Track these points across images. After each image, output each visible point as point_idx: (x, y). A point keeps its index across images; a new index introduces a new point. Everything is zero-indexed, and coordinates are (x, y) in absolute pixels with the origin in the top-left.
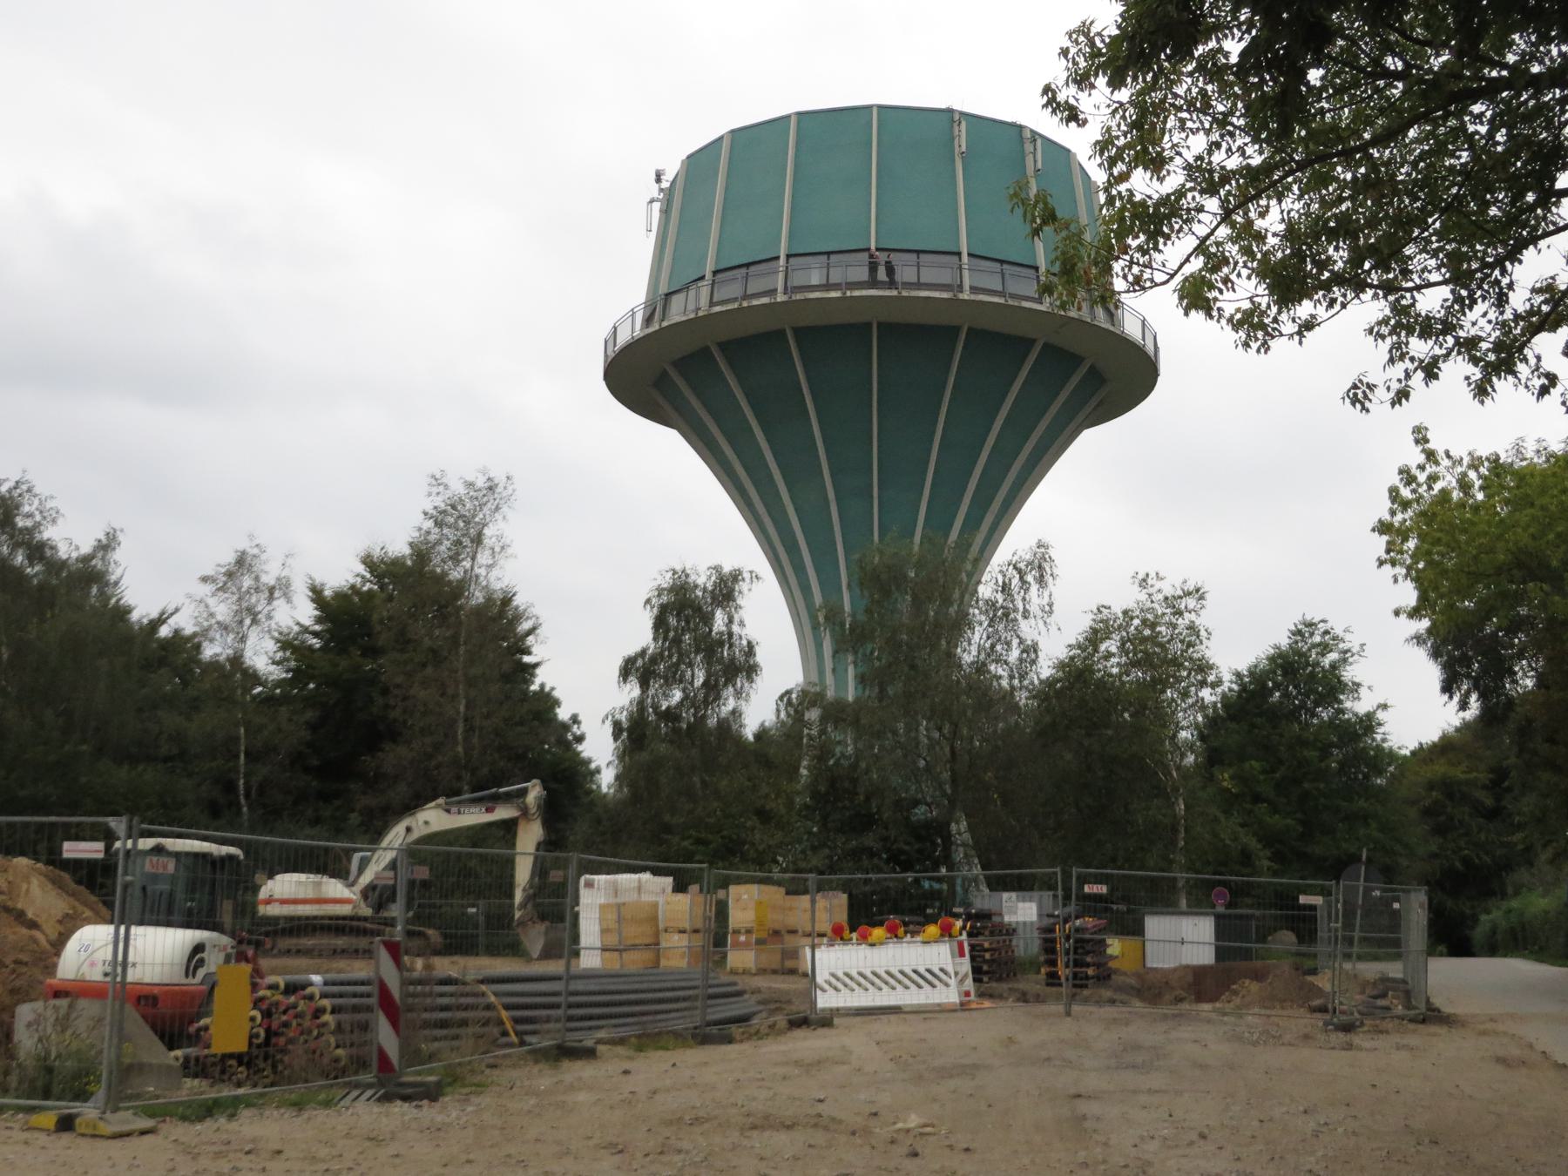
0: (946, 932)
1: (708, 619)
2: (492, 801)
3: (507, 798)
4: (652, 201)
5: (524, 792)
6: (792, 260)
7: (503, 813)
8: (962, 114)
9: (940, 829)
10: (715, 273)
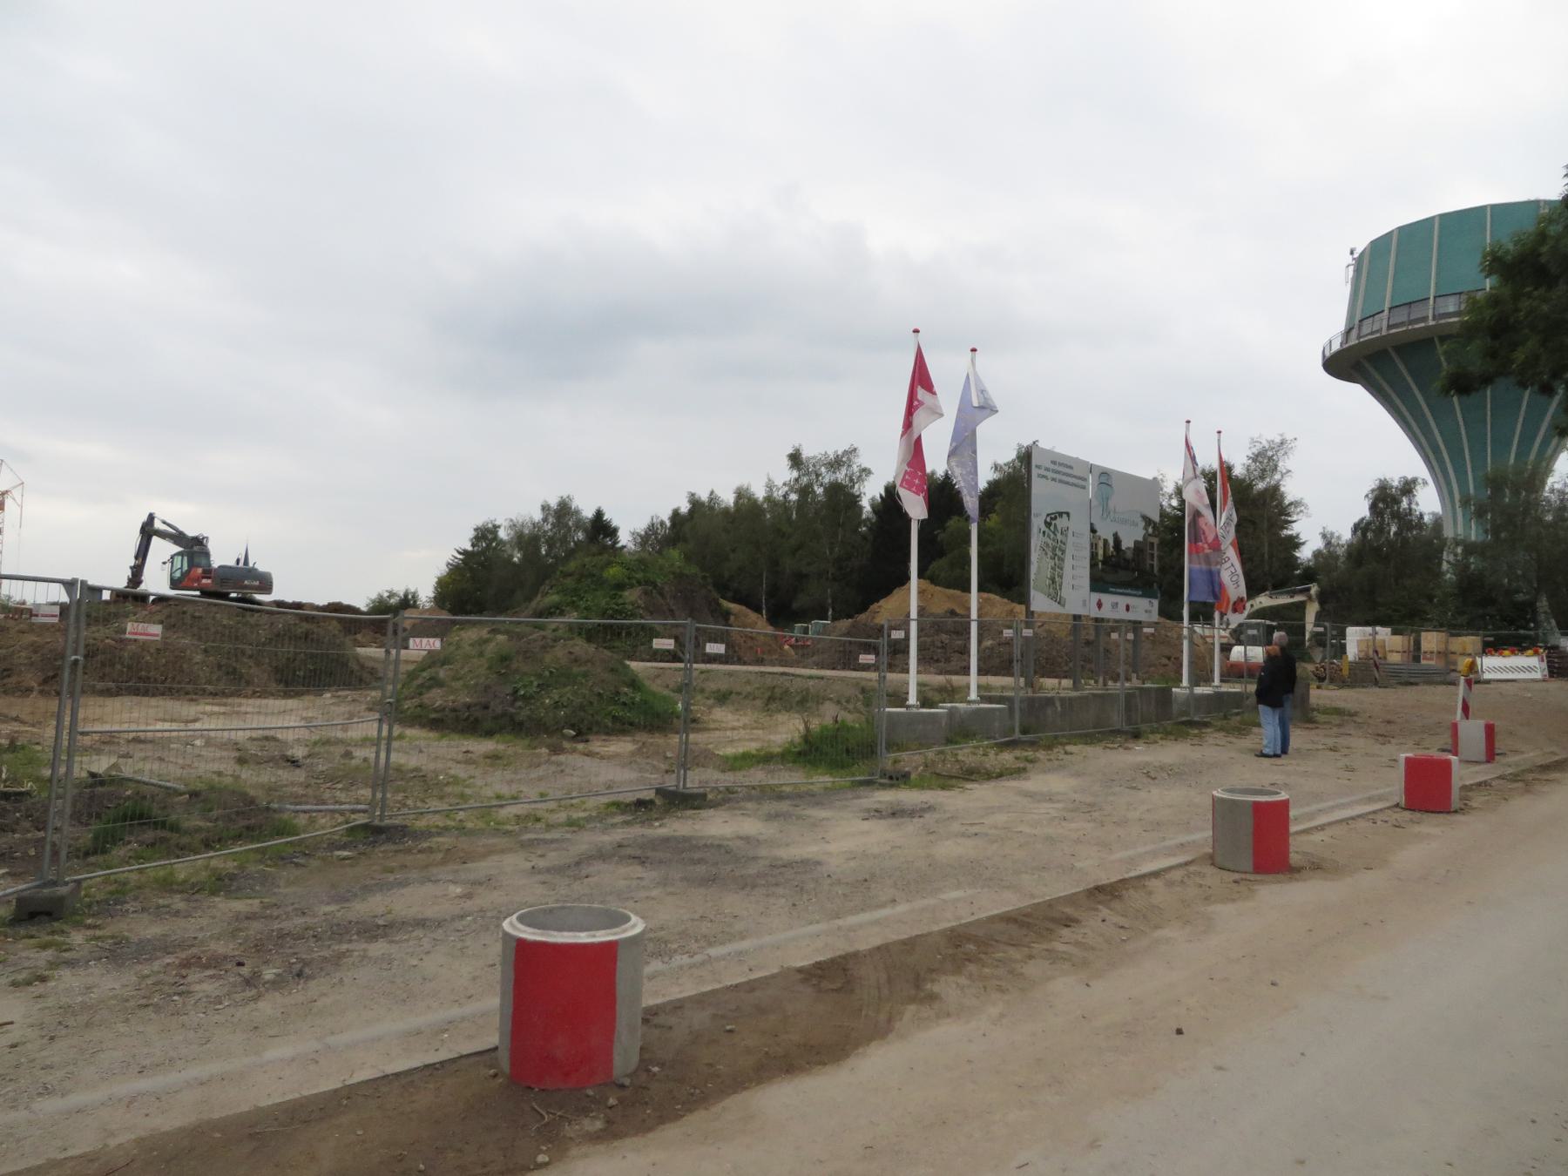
0: (1536, 653)
1: (1398, 502)
2: (1292, 594)
3: (1301, 592)
5: (1308, 590)
7: (1298, 598)
9: (1531, 605)
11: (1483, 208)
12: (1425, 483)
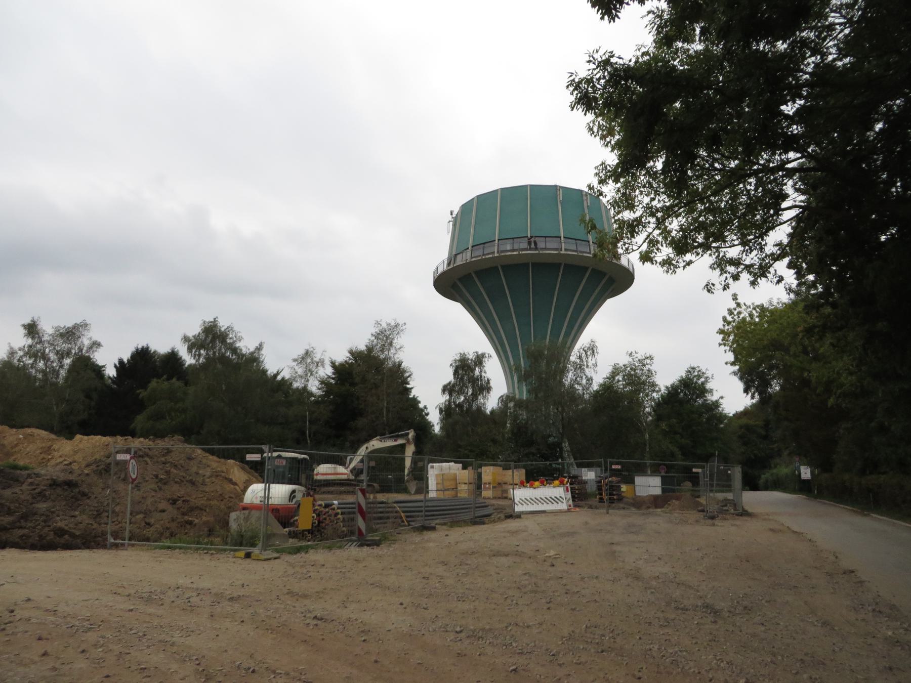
0: (562, 483)
1: (473, 370)
5: (408, 434)
7: (400, 441)
9: (558, 445)
11: (526, 186)
12: (490, 356)
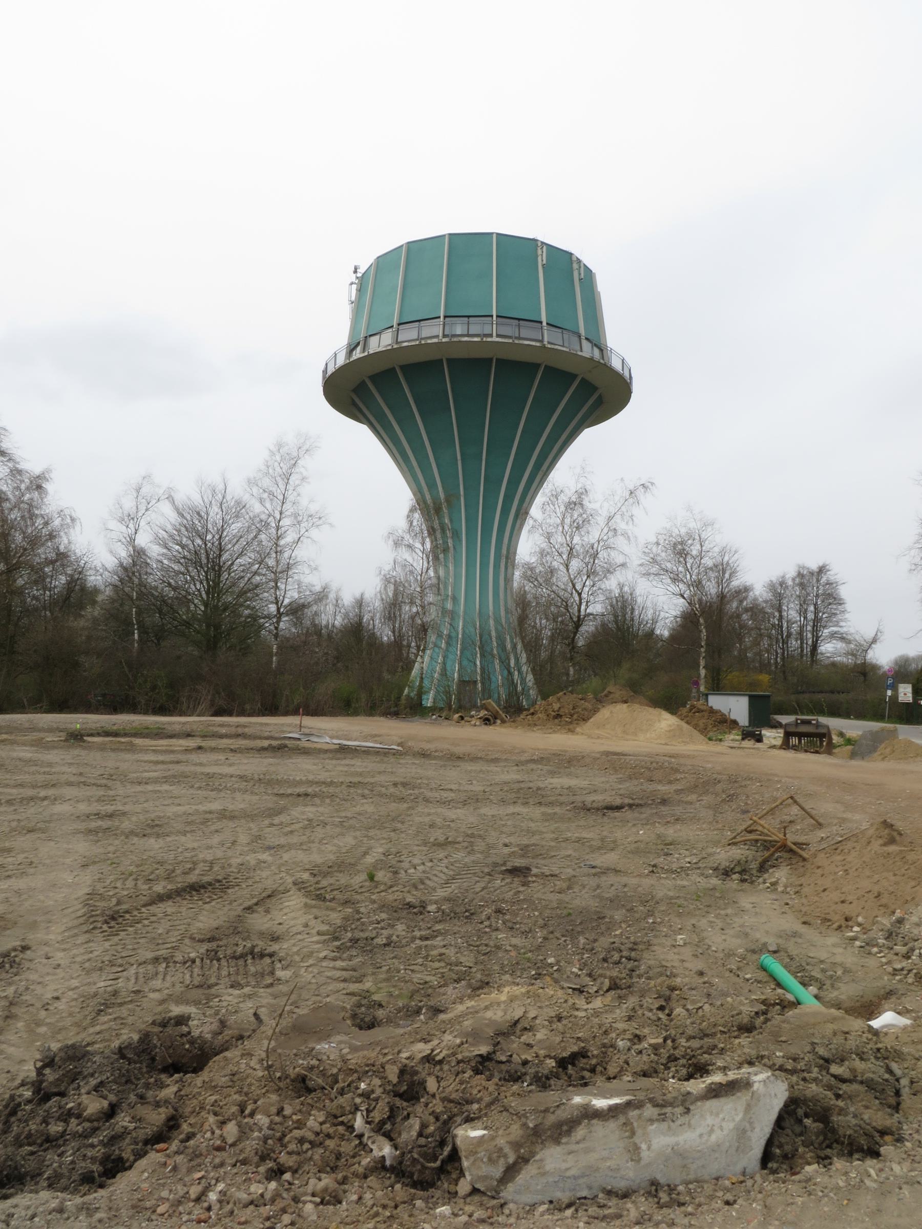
4: (352, 284)
6: (447, 319)
8: (543, 243)
10: (399, 324)
